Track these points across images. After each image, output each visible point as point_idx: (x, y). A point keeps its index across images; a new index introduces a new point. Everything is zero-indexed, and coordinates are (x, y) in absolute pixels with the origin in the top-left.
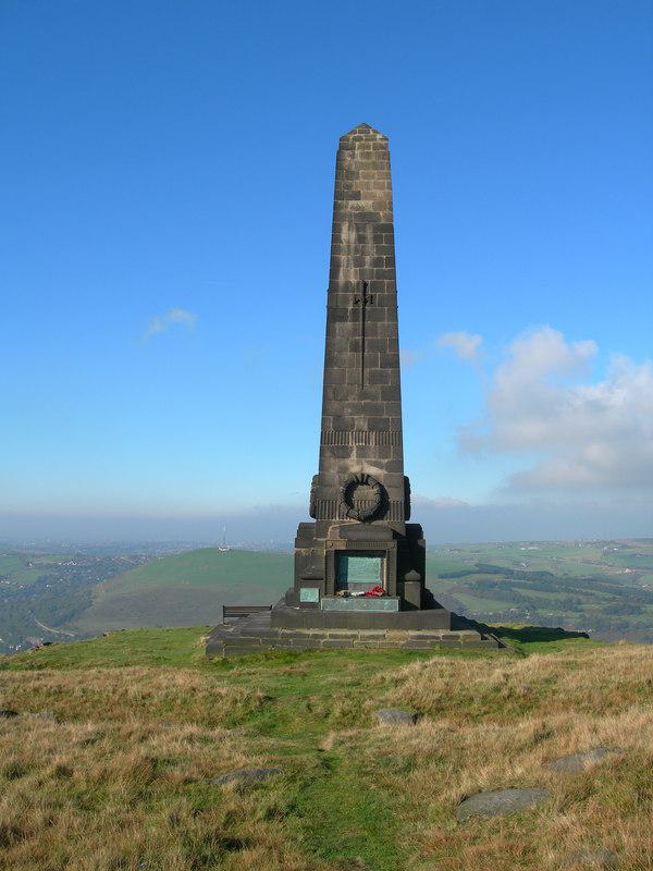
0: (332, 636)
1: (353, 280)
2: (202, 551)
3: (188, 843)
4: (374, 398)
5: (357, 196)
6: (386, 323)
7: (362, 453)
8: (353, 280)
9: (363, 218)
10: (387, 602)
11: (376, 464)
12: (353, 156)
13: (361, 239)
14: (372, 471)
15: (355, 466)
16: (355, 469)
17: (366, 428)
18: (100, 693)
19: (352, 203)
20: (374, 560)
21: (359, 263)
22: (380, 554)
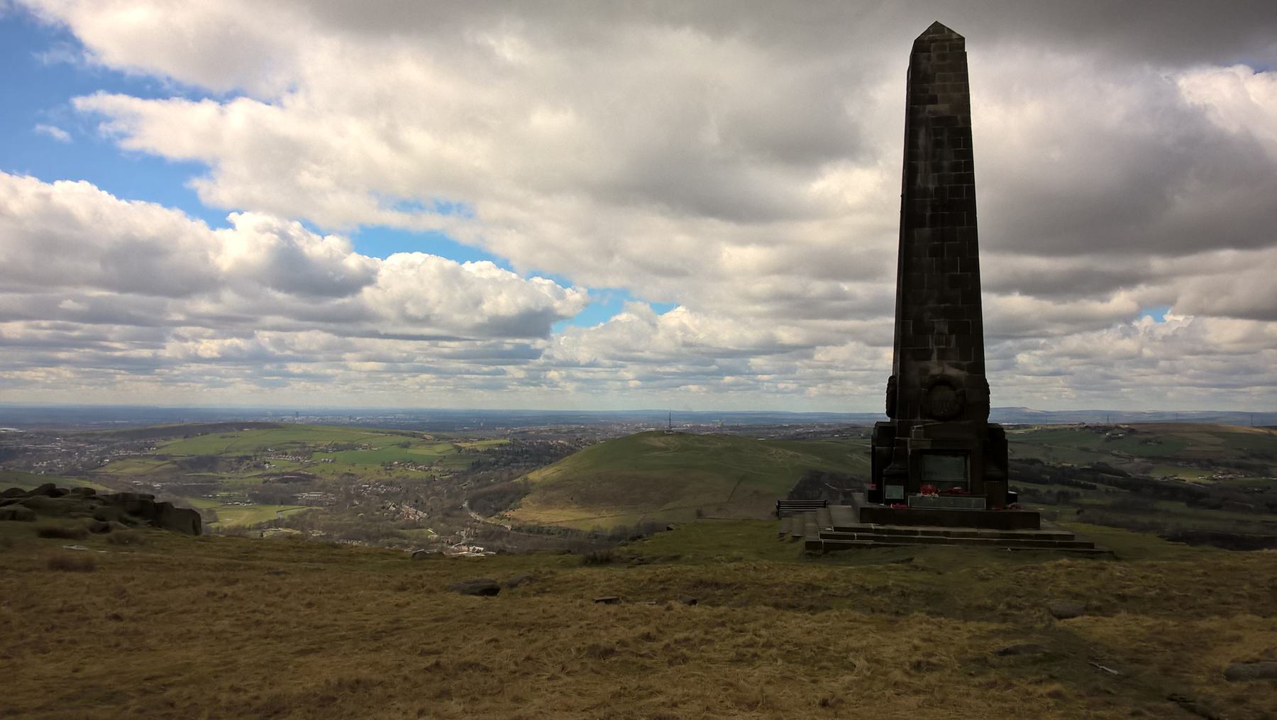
0: (924, 533)
1: (931, 186)
2: (1098, 430)
3: (768, 640)
4: (380, 595)
5: (934, 100)
6: (928, 258)
7: (943, 356)
8: (931, 186)
9: (940, 120)
10: (974, 500)
11: (958, 366)
12: (929, 59)
13: (938, 144)
14: (952, 372)
15: (935, 367)
16: (935, 370)
17: (946, 331)
18: (592, 355)
19: (930, 107)
20: (958, 459)
21: (937, 168)
22: (1011, 460)
